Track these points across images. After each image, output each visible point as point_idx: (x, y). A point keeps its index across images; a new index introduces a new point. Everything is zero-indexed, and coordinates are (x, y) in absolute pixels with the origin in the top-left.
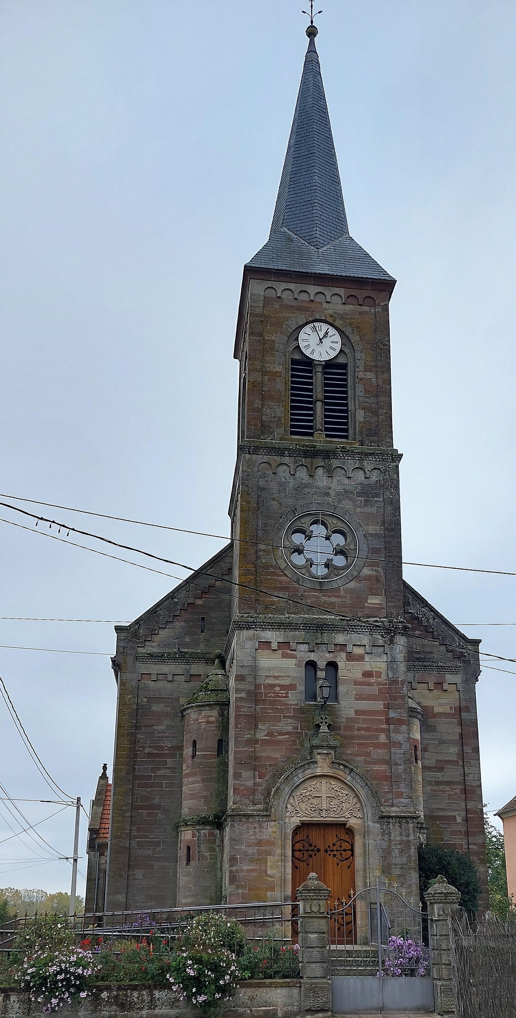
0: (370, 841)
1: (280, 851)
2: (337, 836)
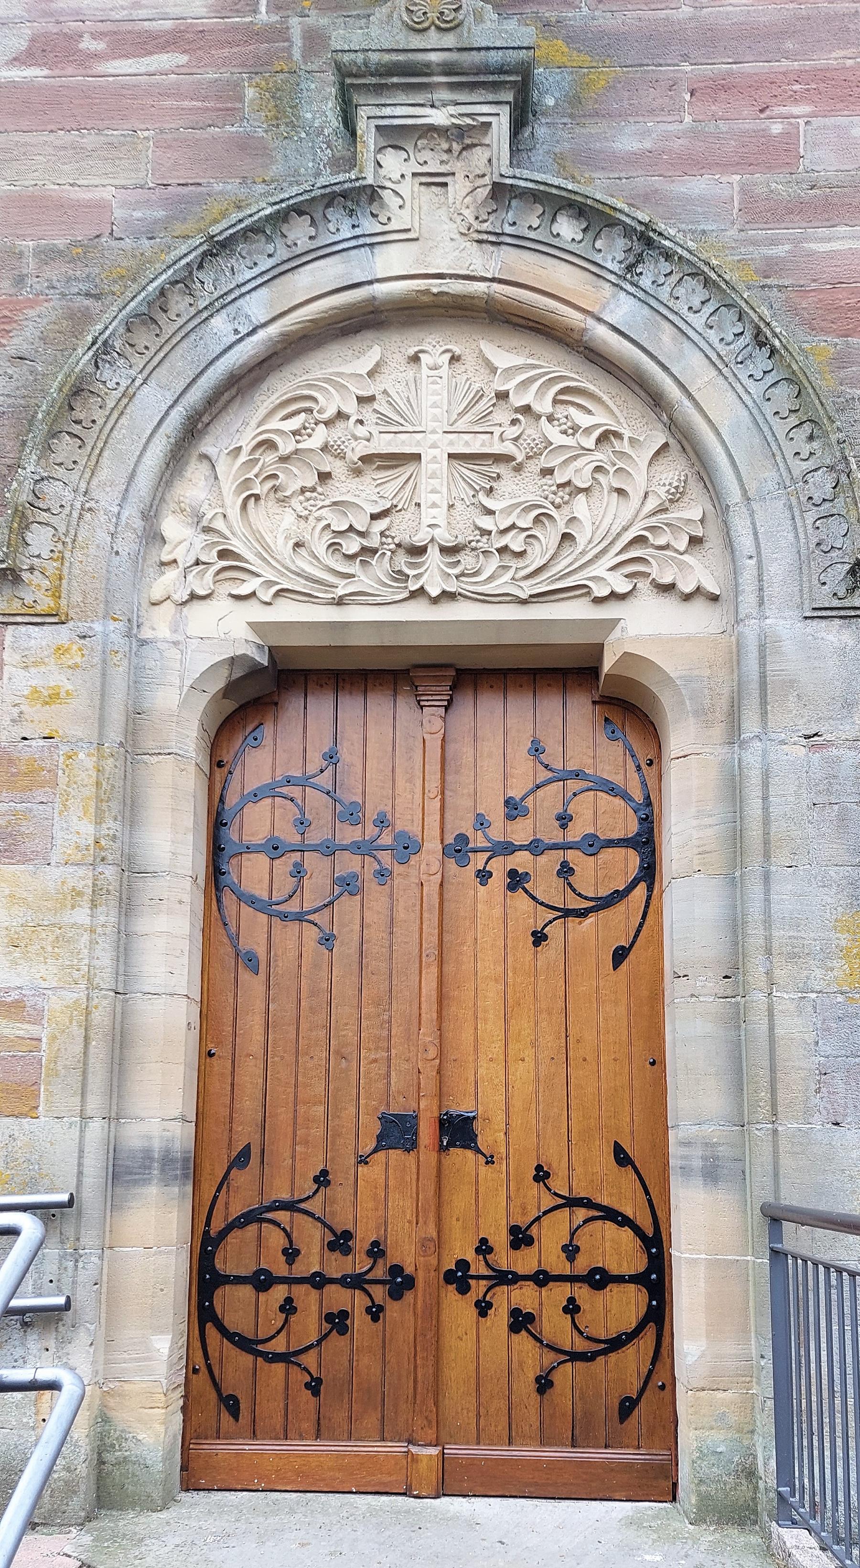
0: (782, 758)
1: (87, 830)
2: (537, 750)
